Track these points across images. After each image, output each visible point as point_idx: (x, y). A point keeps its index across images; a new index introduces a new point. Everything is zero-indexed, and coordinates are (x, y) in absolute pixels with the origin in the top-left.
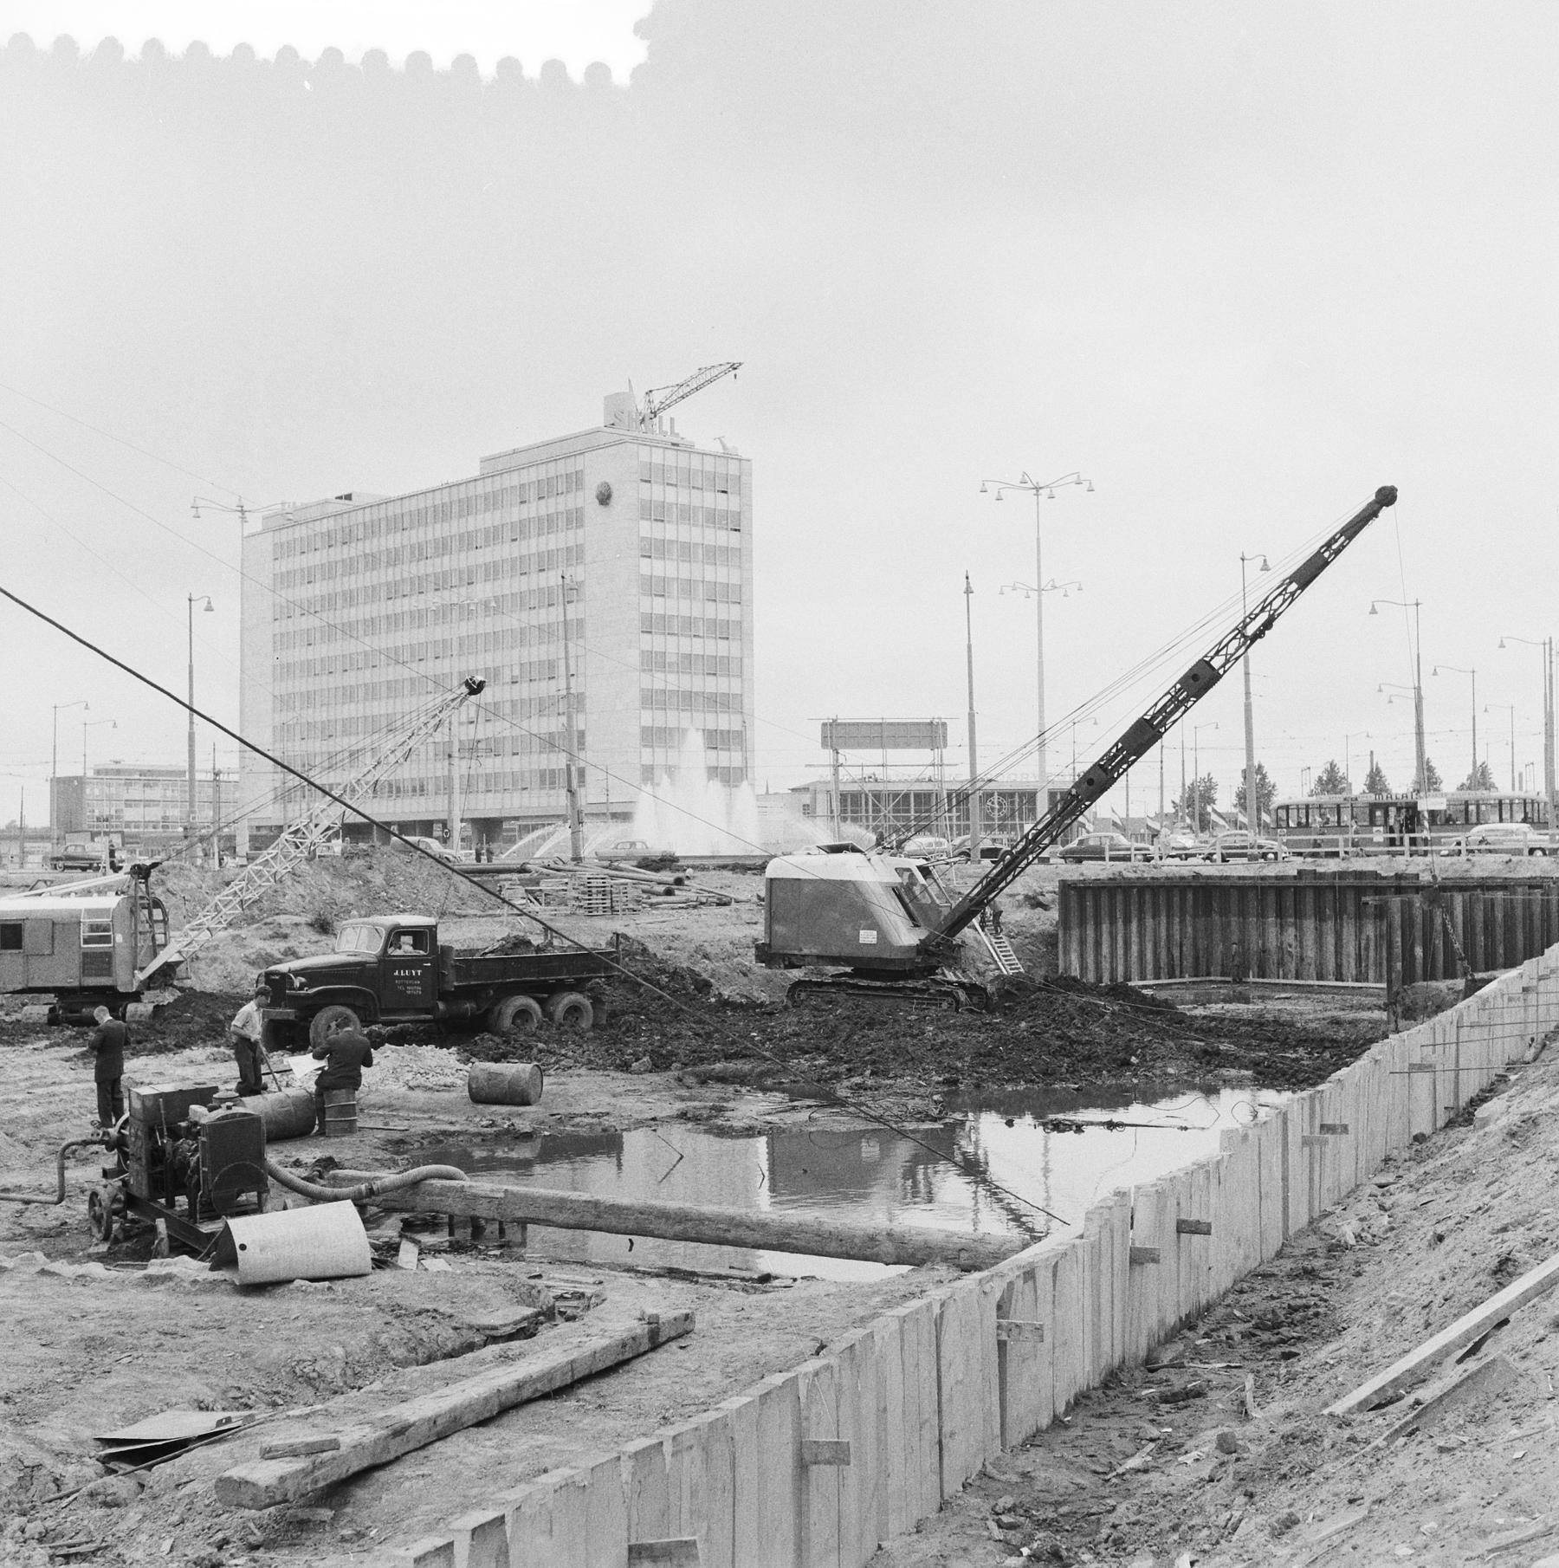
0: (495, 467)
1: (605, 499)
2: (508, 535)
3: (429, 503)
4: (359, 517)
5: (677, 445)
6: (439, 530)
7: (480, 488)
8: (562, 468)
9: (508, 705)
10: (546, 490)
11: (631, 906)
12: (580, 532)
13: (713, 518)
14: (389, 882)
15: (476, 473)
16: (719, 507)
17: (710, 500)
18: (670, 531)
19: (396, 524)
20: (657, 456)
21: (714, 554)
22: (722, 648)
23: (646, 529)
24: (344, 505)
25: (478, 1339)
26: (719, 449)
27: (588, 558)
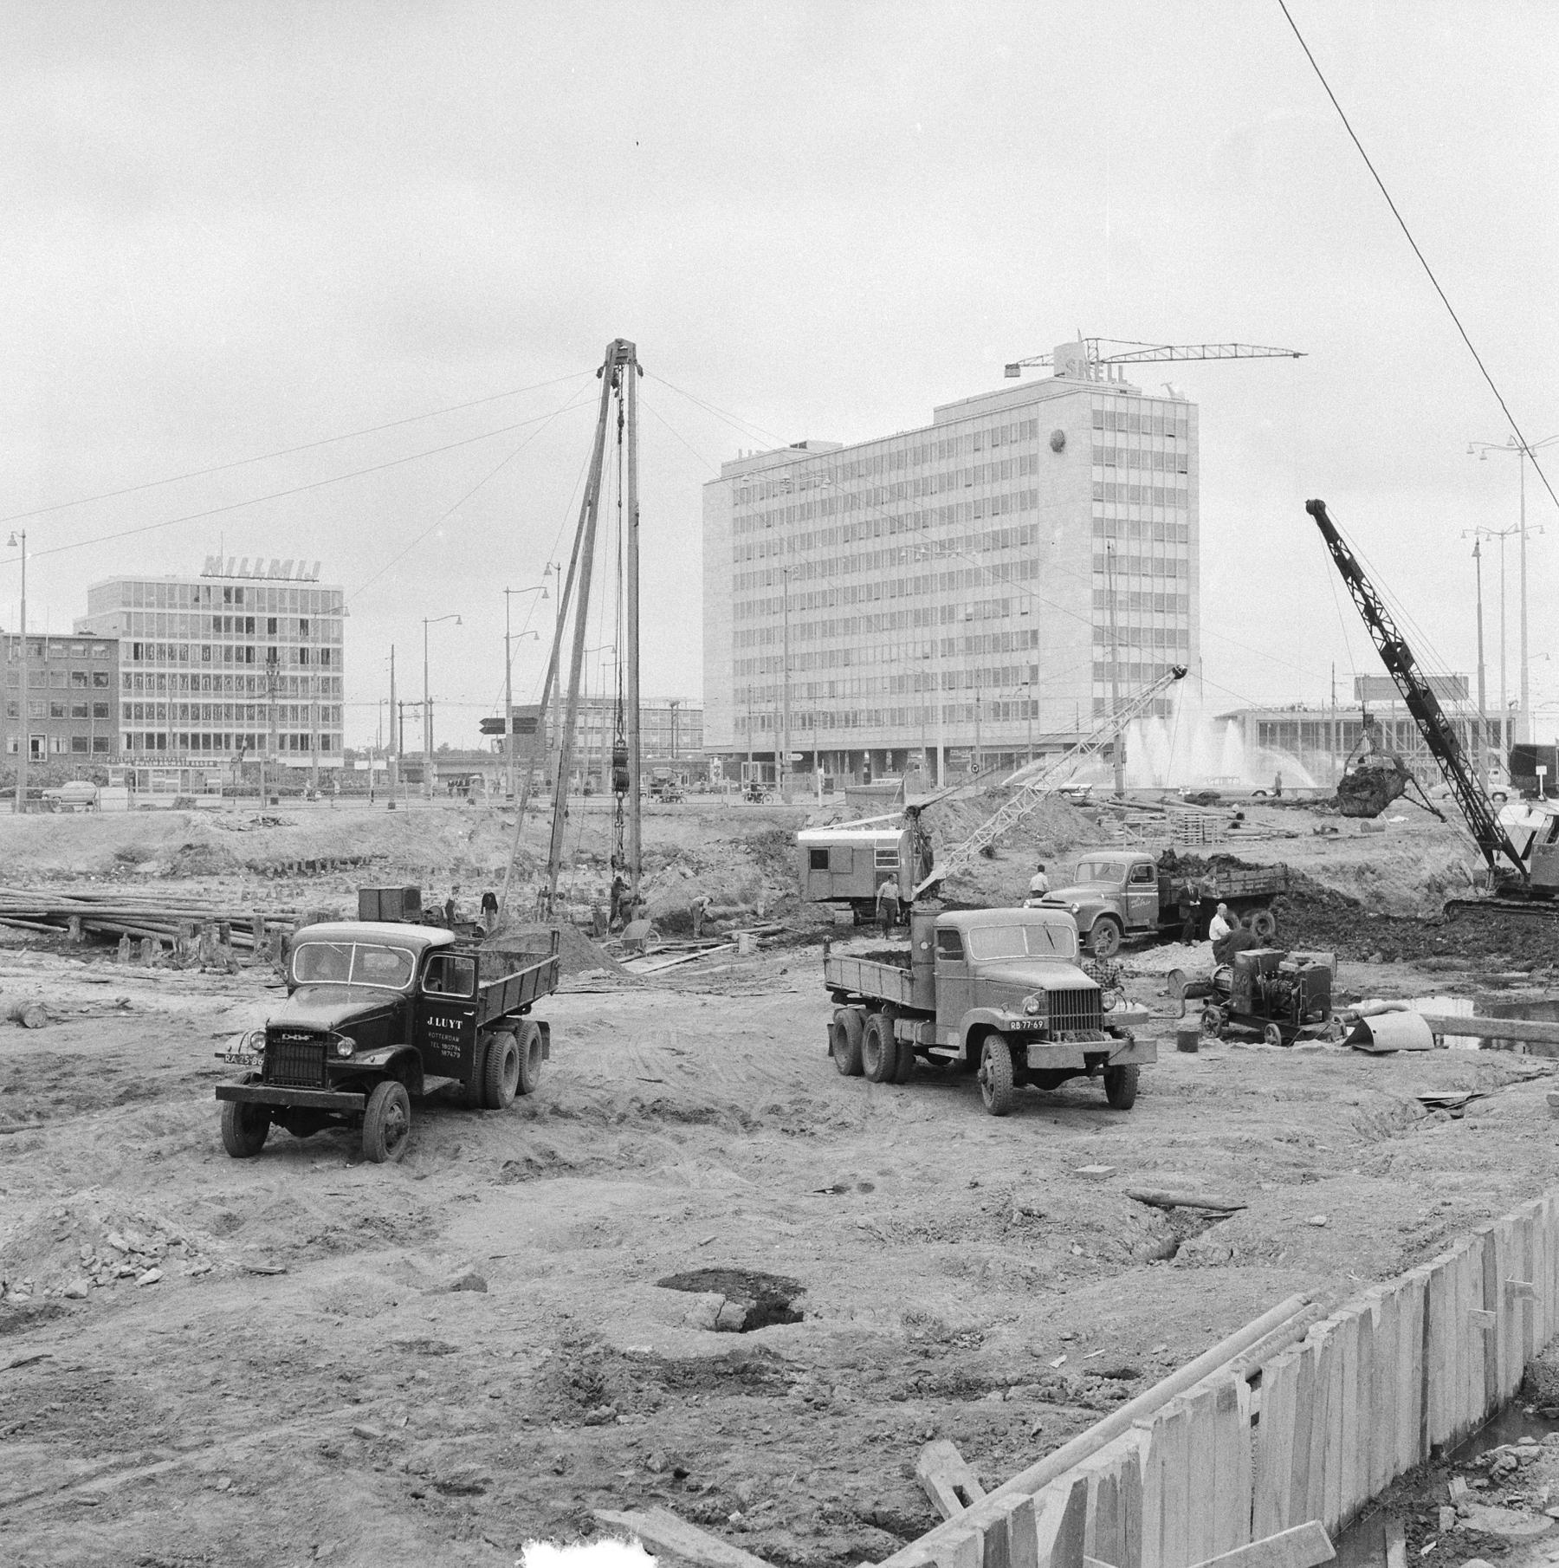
0: (947, 416)
1: (1058, 446)
2: (962, 481)
3: (885, 451)
4: (817, 465)
5: (1125, 392)
6: (893, 477)
7: (934, 437)
8: (1017, 417)
10: (999, 438)
12: (1034, 478)
13: (1162, 462)
15: (930, 423)
16: (1178, 451)
17: (1158, 444)
18: (1121, 476)
19: (851, 471)
20: (1109, 405)
21: (1162, 497)
22: (1169, 586)
23: (1098, 474)
24: (799, 455)
25: (1520, 1078)
26: (1166, 395)
27: (1042, 502)
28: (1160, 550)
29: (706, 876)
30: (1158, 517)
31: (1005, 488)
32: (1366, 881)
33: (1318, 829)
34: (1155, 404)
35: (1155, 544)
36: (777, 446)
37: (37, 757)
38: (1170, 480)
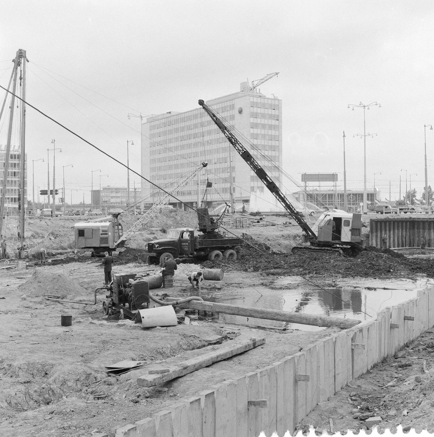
1: (240, 112)
4: (173, 118)
8: (228, 103)
9: (214, 170)
11: (248, 226)
13: (271, 117)
14: (182, 219)
17: (270, 112)
18: (259, 121)
19: (183, 120)
20: (255, 100)
21: (271, 127)
23: (252, 120)
24: (169, 115)
25: (206, 344)
29: (58, 239)
30: (270, 133)
32: (297, 240)
33: (285, 223)
35: (269, 141)
36: (162, 113)
38: (274, 122)
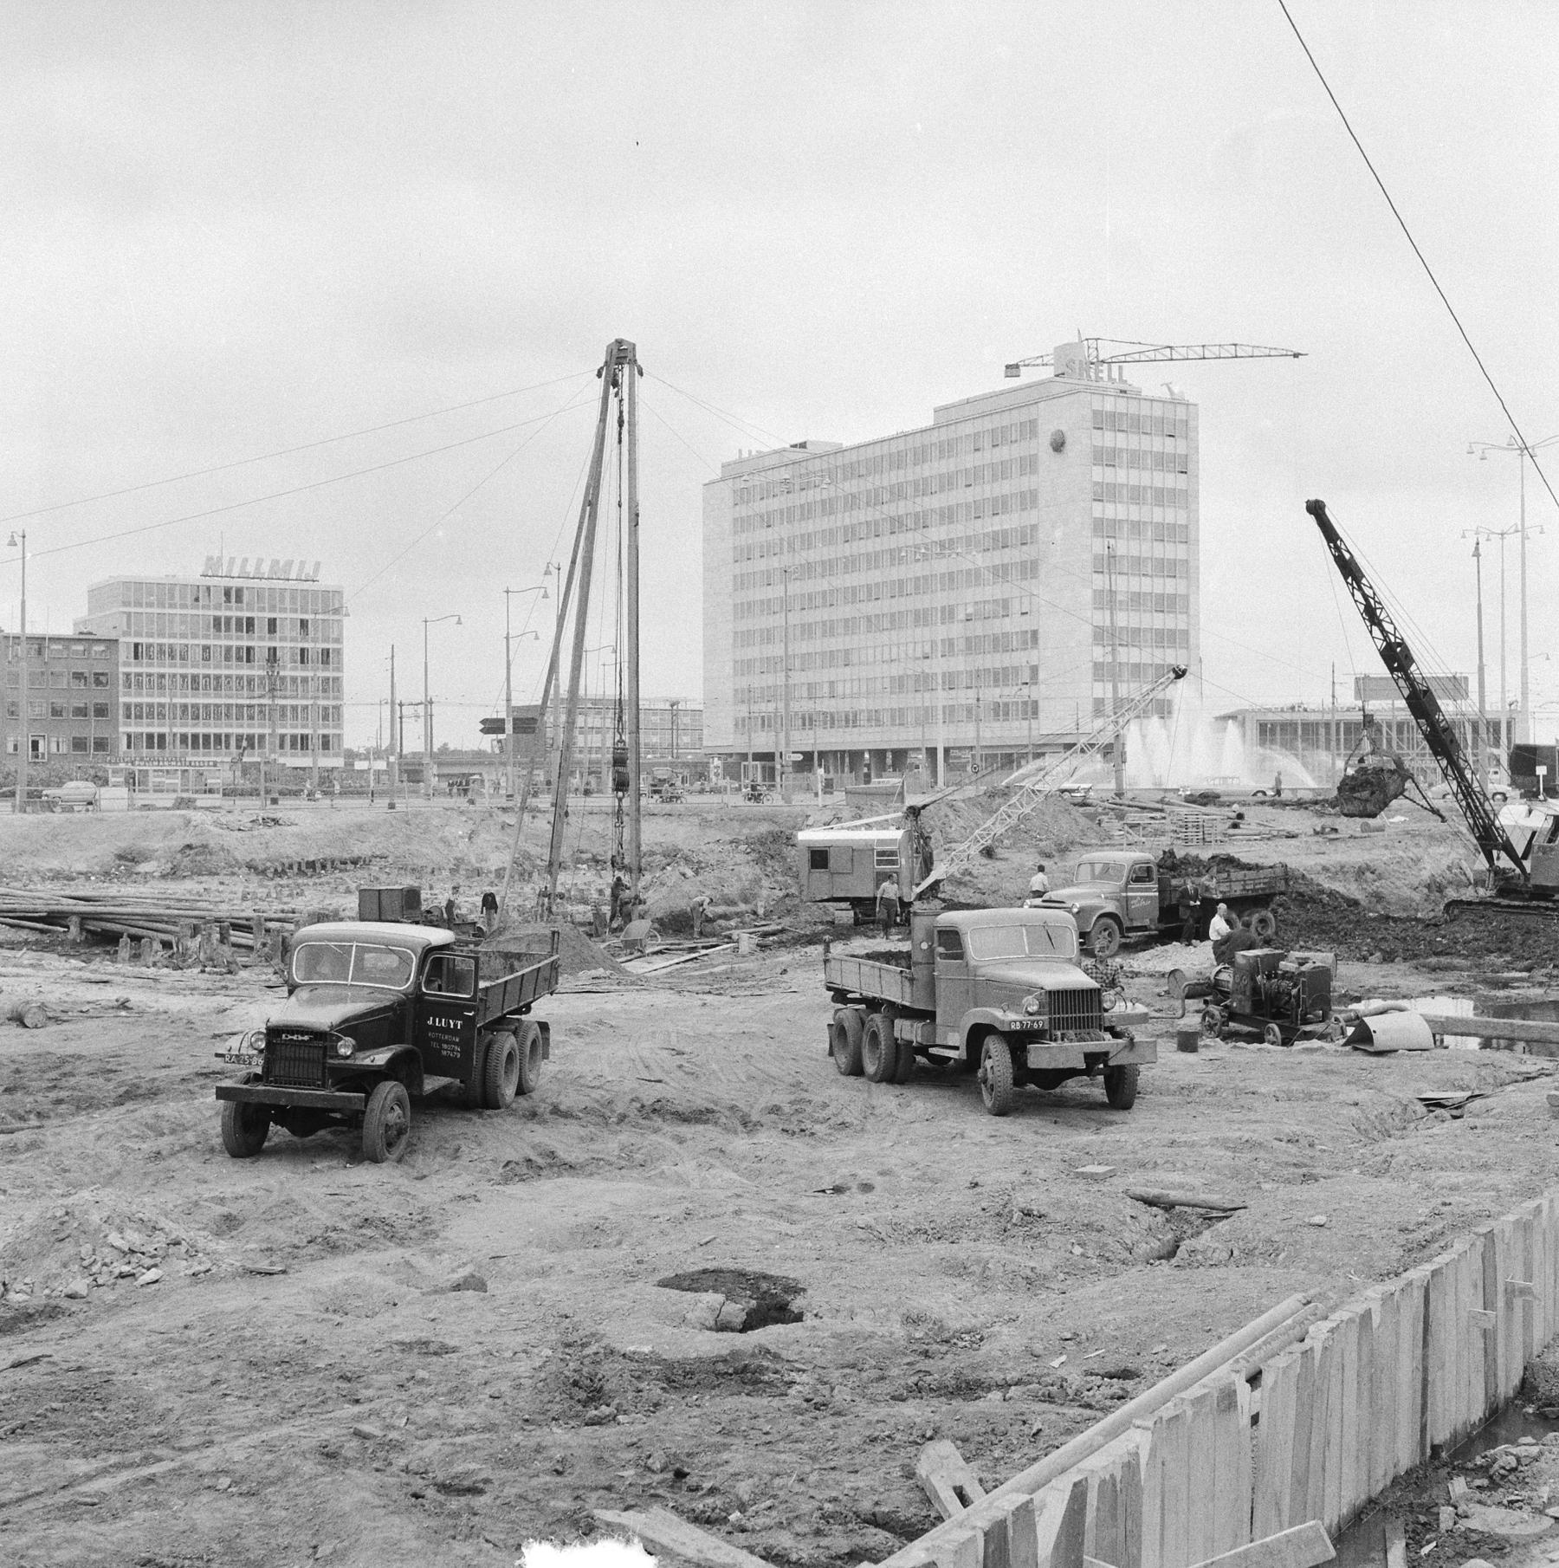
0: (947, 416)
1: (1058, 446)
4: (817, 465)
8: (1017, 417)
10: (999, 438)
13: (1162, 462)
17: (1158, 444)
18: (1121, 476)
19: (851, 471)
20: (1109, 405)
21: (1162, 497)
22: (1169, 586)
23: (1098, 474)
24: (799, 455)
25: (1520, 1078)
26: (1166, 395)
28: (1160, 550)
30: (1158, 517)
31: (1005, 488)
32: (1366, 881)
34: (1155, 404)
35: (1155, 544)
36: (777, 446)
37: (37, 757)
38: (1170, 480)
